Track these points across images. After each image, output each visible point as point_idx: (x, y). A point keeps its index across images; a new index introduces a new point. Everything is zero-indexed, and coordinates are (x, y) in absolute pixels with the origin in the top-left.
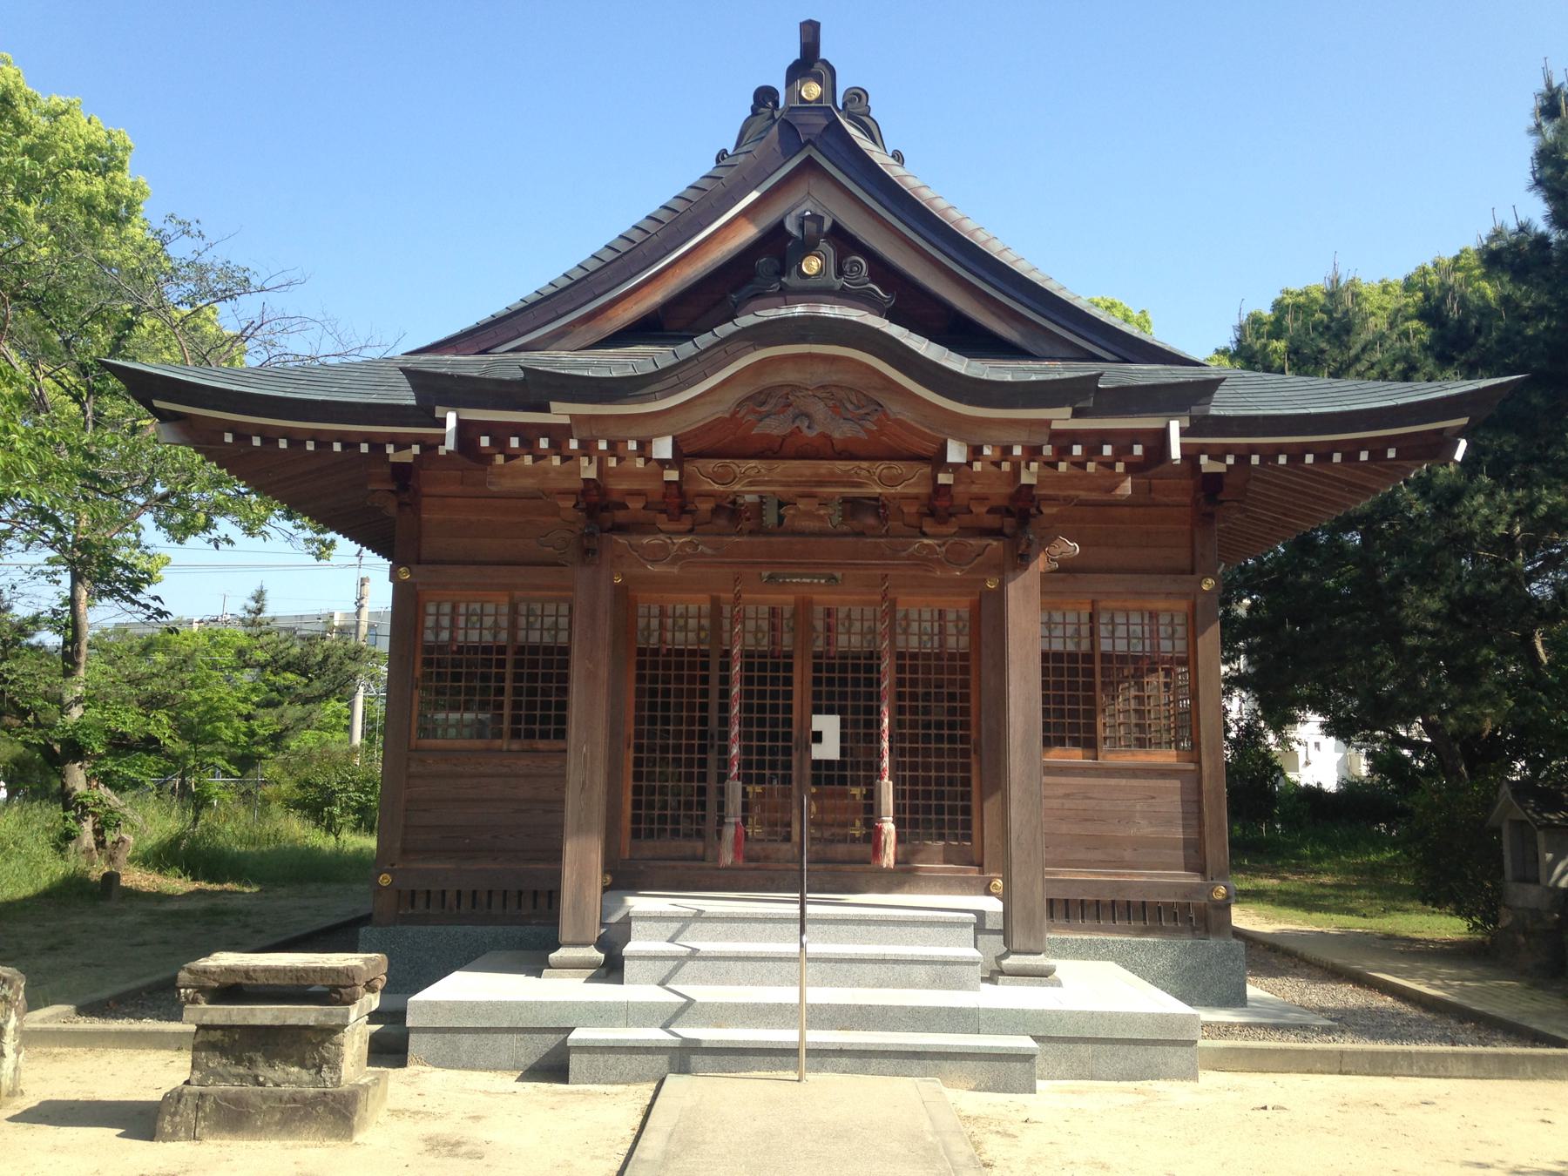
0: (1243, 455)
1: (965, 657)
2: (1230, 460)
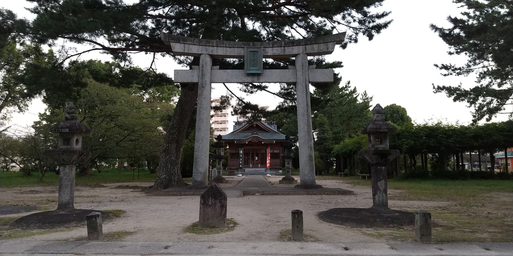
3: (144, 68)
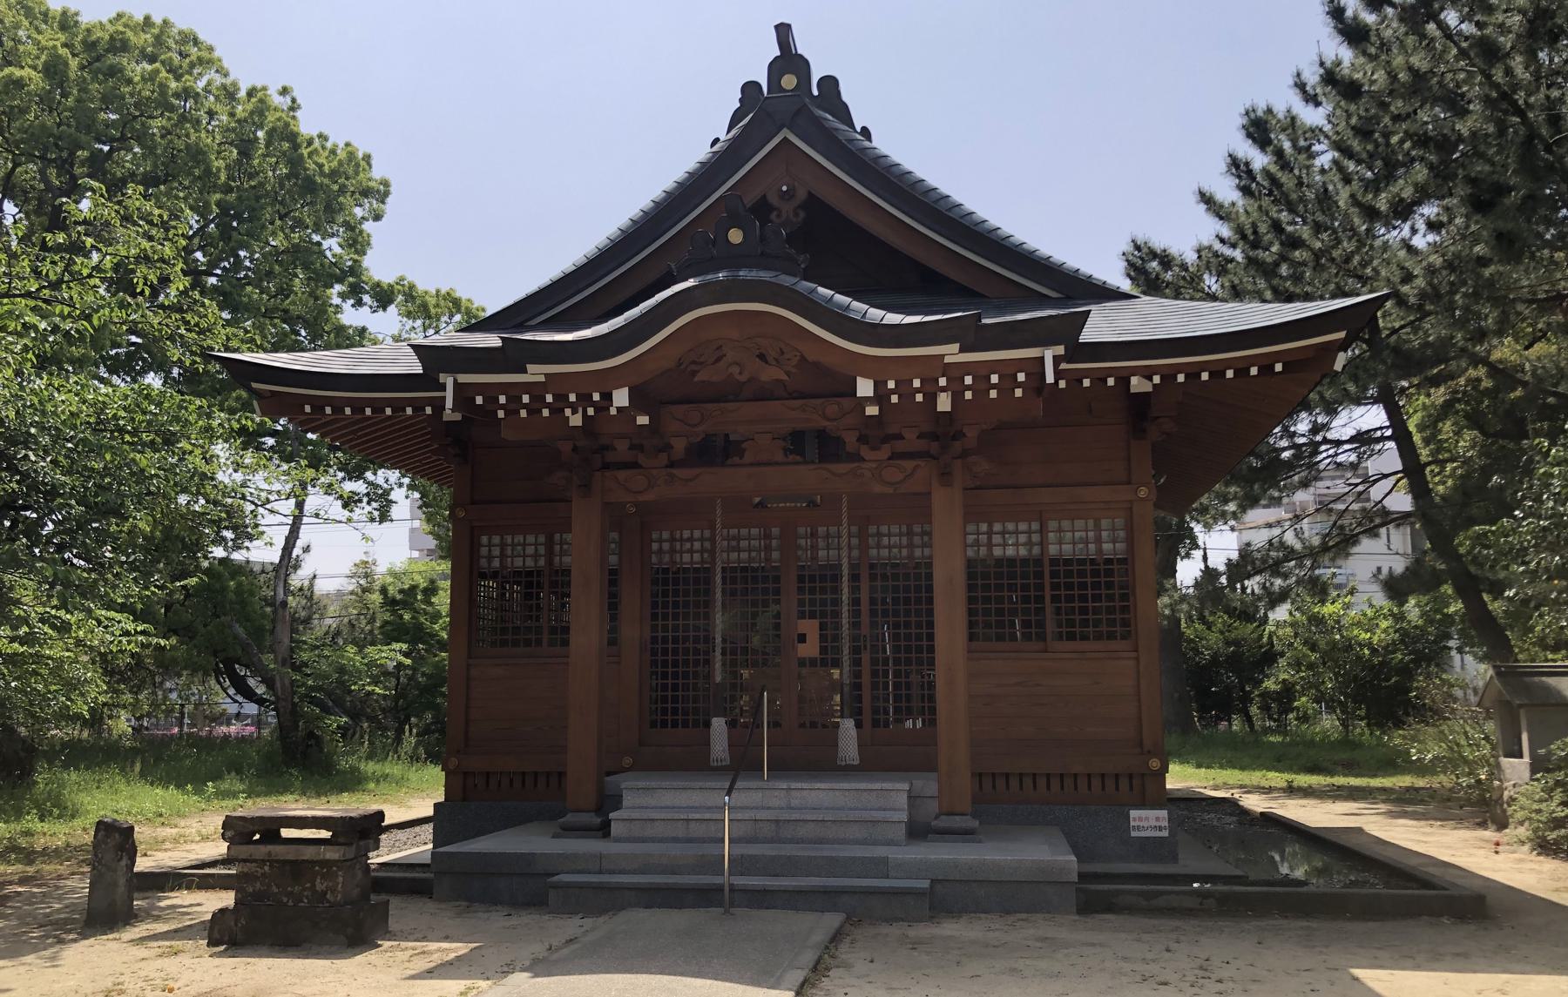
0: (1169, 375)
1: (1123, 561)
2: (1157, 379)
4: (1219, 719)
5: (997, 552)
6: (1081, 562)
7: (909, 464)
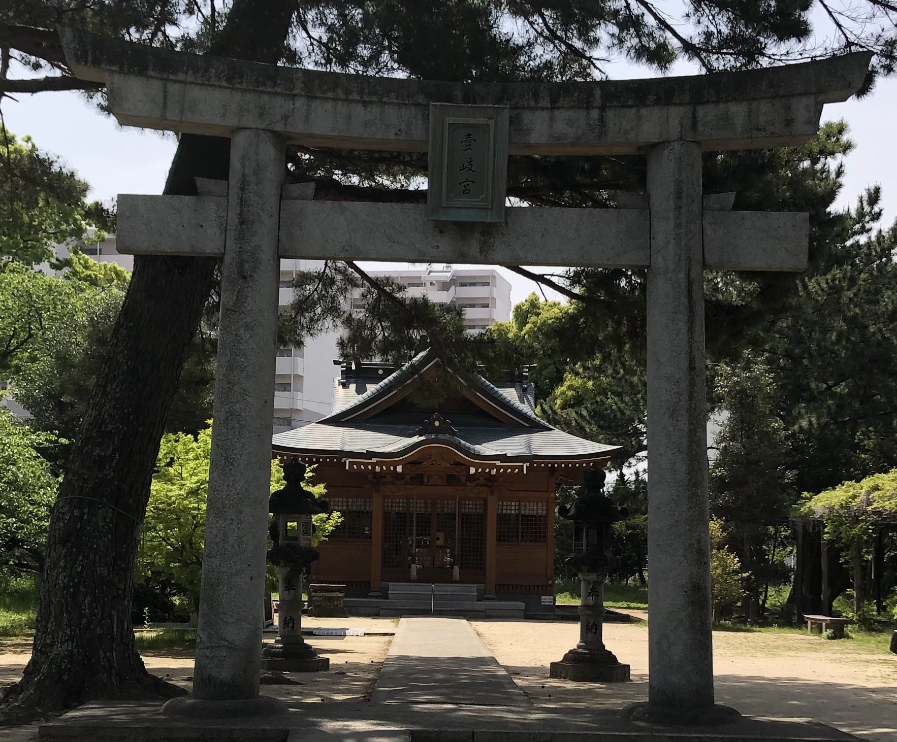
1: (545, 517)
3: (566, 596)
4: (621, 579)
5: (504, 512)
6: (532, 516)
7: (481, 488)
